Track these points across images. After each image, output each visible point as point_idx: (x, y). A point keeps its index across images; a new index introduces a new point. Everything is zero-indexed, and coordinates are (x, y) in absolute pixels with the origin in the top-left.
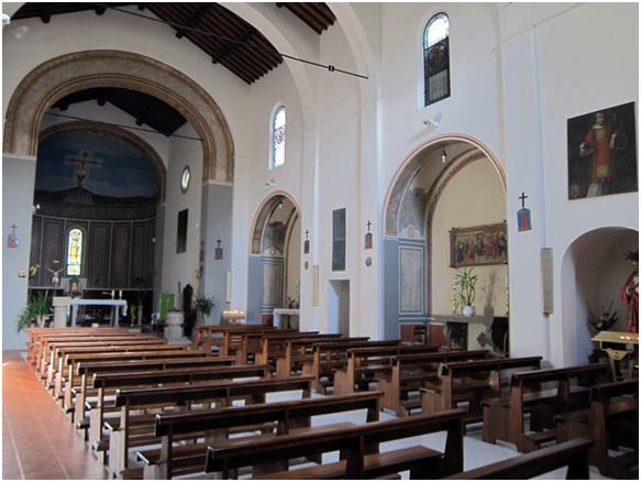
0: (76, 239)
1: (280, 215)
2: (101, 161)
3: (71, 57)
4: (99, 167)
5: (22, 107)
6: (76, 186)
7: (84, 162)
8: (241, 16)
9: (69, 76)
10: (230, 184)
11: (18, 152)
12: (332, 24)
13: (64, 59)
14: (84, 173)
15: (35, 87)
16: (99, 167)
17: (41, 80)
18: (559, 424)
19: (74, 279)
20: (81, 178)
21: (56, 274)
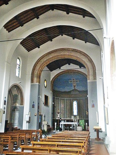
0: (75, 104)
1: (15, 92)
2: (78, 80)
3: (45, 55)
4: (78, 82)
5: (35, 71)
6: (74, 89)
7: (74, 82)
8: (70, 37)
9: (45, 60)
10: (95, 81)
11: (34, 82)
12: (51, 41)
13: (44, 56)
14: (75, 85)
15: (38, 65)
16: (78, 82)
17: (39, 63)
18: (90, 135)
19: (75, 116)
20: (75, 86)
21: (58, 115)
